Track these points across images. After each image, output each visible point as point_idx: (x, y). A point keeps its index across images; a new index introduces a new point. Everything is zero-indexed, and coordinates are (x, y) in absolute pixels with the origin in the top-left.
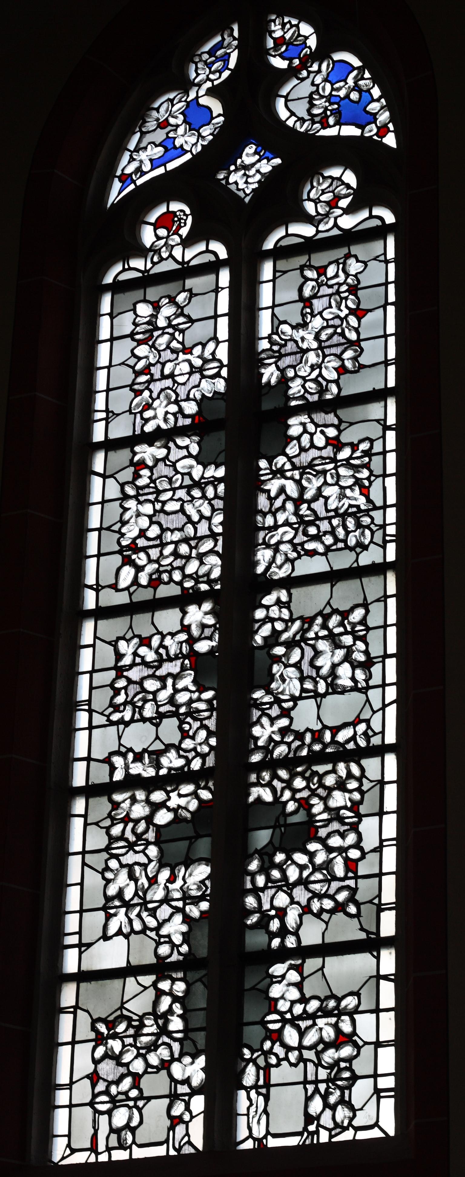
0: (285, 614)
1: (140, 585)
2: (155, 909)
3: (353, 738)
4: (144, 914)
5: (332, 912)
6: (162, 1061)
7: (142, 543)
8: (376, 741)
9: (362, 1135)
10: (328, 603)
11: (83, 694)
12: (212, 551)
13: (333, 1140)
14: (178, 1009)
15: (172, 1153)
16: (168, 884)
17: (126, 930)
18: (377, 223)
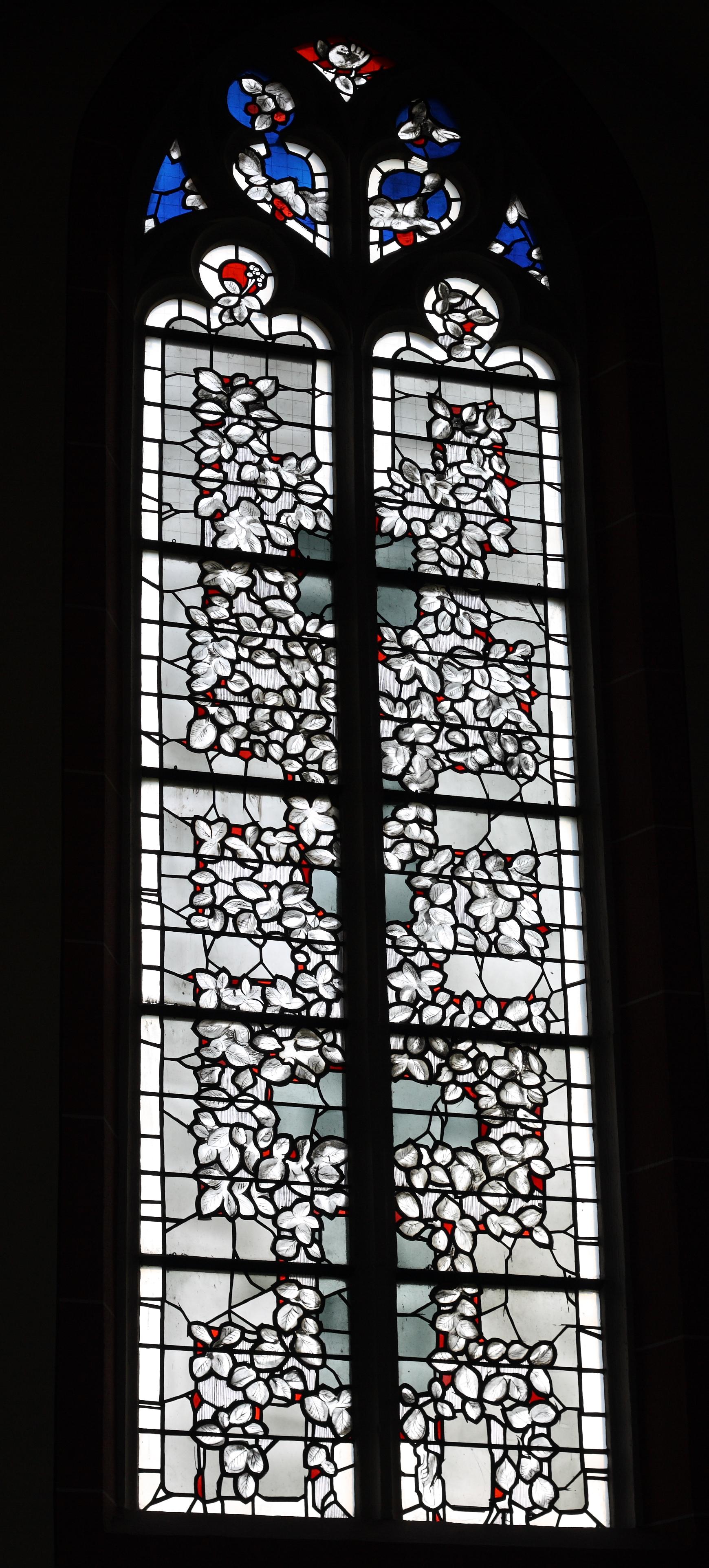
0: (428, 837)
1: (222, 751)
2: (271, 1191)
3: (529, 1018)
4: (254, 1193)
5: (516, 1236)
6: (294, 1391)
7: (222, 694)
8: (557, 1028)
9: (568, 1522)
10: (485, 838)
11: (149, 879)
12: (322, 732)
13: (532, 1523)
14: (311, 1325)
15: (313, 1514)
16: (287, 1161)
17: (230, 1209)
18: (523, 372)
